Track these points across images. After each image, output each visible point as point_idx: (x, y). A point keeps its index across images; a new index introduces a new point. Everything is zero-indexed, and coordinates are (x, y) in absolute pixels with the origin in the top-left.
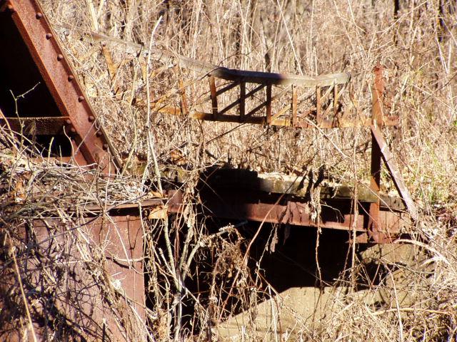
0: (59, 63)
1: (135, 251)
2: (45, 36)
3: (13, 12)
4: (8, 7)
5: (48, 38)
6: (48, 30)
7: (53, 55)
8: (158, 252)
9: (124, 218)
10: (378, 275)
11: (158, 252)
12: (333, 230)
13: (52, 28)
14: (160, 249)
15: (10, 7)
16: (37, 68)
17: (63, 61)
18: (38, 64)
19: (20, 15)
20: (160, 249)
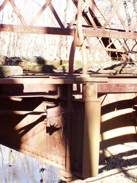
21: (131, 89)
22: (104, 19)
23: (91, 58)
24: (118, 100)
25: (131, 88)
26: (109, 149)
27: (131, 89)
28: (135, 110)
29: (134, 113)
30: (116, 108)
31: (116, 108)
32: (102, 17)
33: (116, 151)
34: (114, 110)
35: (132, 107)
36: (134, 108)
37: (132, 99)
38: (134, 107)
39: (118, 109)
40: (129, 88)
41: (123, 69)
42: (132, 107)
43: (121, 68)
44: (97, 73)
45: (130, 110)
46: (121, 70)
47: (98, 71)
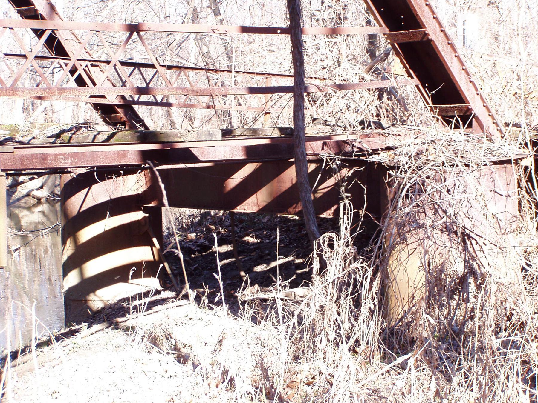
0: (463, 72)
1: (510, 186)
2: (454, 55)
3: (431, 40)
4: (428, 38)
5: (456, 56)
6: (456, 52)
7: (459, 66)
8: (528, 185)
9: (503, 166)
10: (472, 119)
11: (528, 185)
12: (168, 200)
13: (458, 50)
14: (529, 183)
15: (430, 37)
16: (437, 55)
17: (477, 235)
18: (449, 73)
19: (437, 43)
20: (529, 183)
21: (66, 163)
22: (77, 41)
23: (394, 133)
24: (113, 197)
25: (66, 161)
26: (99, 292)
27: (66, 163)
28: (147, 215)
29: (145, 221)
30: (108, 212)
31: (108, 212)
32: (75, 39)
33: (115, 296)
34: (104, 217)
35: (141, 210)
36: (146, 210)
37: (140, 193)
38: (145, 207)
39: (112, 215)
40: (63, 162)
41: (74, 136)
42: (140, 210)
43: (70, 135)
44: (28, 143)
45: (138, 215)
46: (71, 138)
47: (30, 141)
